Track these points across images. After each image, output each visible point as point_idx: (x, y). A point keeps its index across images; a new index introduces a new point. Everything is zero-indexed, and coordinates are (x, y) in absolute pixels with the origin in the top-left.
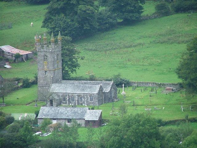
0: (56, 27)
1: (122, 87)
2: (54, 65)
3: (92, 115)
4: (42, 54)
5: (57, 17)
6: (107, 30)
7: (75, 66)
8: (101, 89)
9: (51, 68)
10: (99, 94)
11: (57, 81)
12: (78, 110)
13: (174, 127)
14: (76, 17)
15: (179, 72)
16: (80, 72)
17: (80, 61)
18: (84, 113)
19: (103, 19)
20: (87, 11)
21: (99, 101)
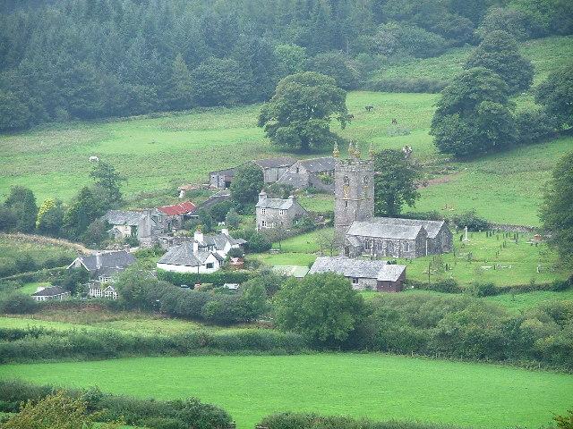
0: (444, 135)
1: (41, 220)
2: (358, 192)
3: (389, 273)
4: (342, 175)
5: (446, 119)
6: (536, 141)
7: (413, 197)
8: (423, 233)
9: (354, 197)
10: (418, 240)
11: (362, 218)
12: (373, 264)
13: (435, 295)
14: (478, 120)
15: (543, 218)
16: (421, 206)
17: (420, 190)
18: (378, 269)
19: (529, 125)
20: (492, 111)
21: (417, 250)
